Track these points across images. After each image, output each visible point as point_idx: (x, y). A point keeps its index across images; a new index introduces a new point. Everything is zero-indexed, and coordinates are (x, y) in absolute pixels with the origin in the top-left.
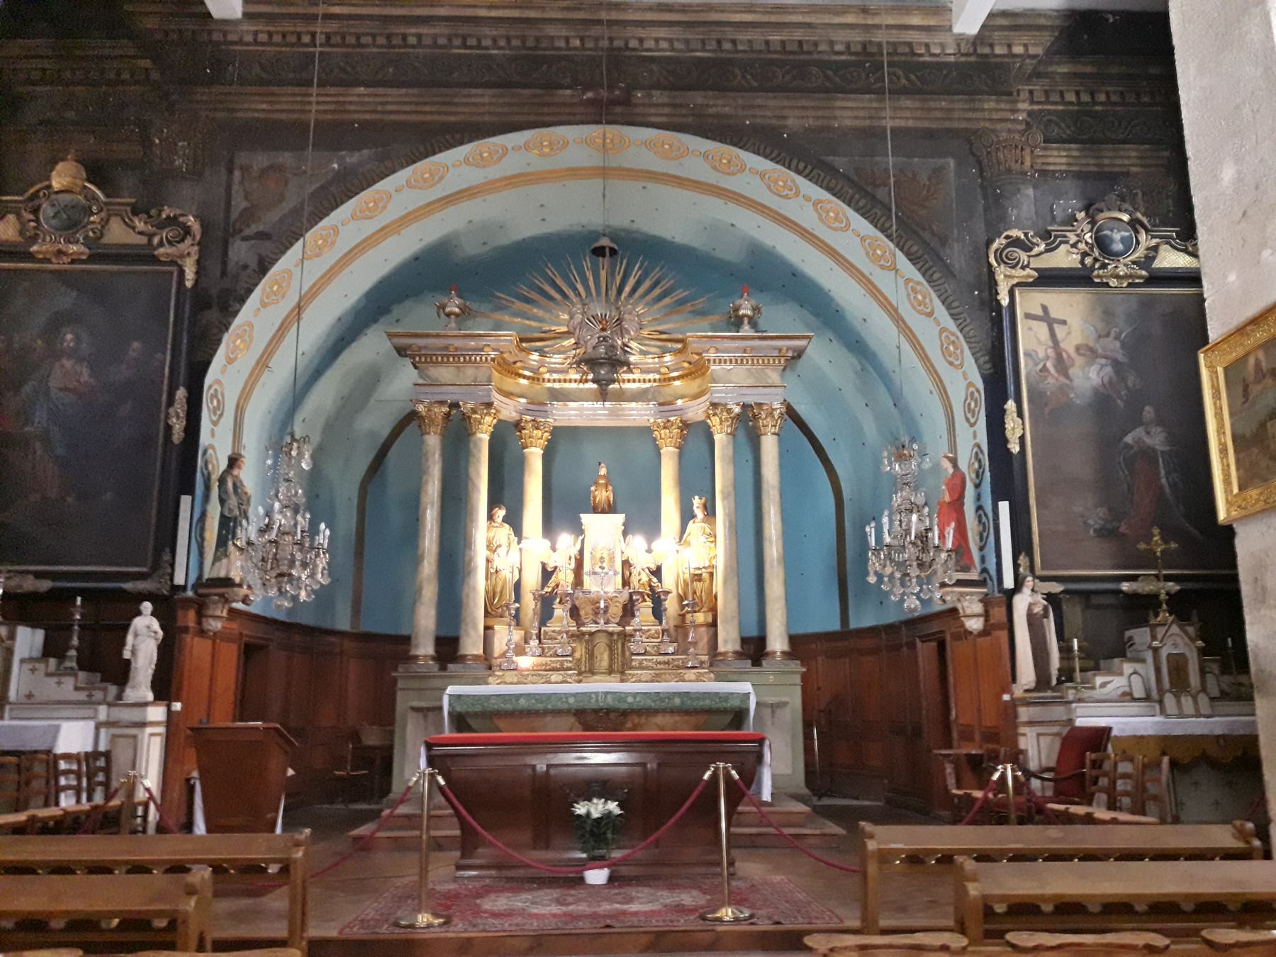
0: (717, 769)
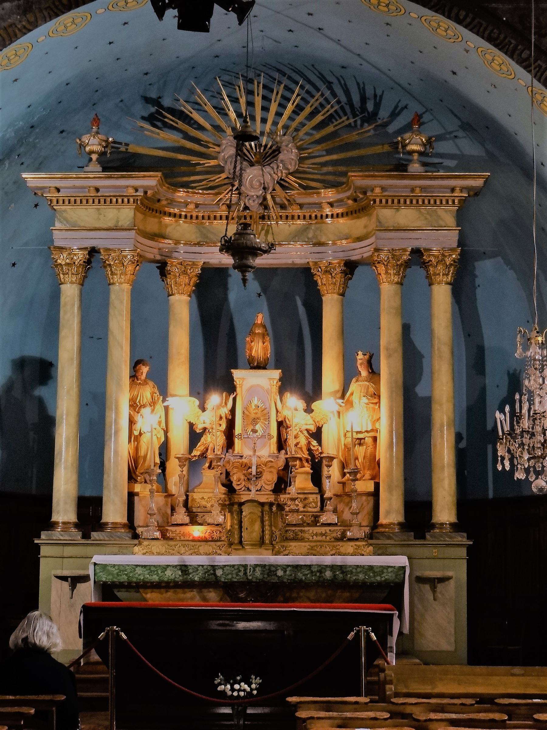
0: (359, 632)
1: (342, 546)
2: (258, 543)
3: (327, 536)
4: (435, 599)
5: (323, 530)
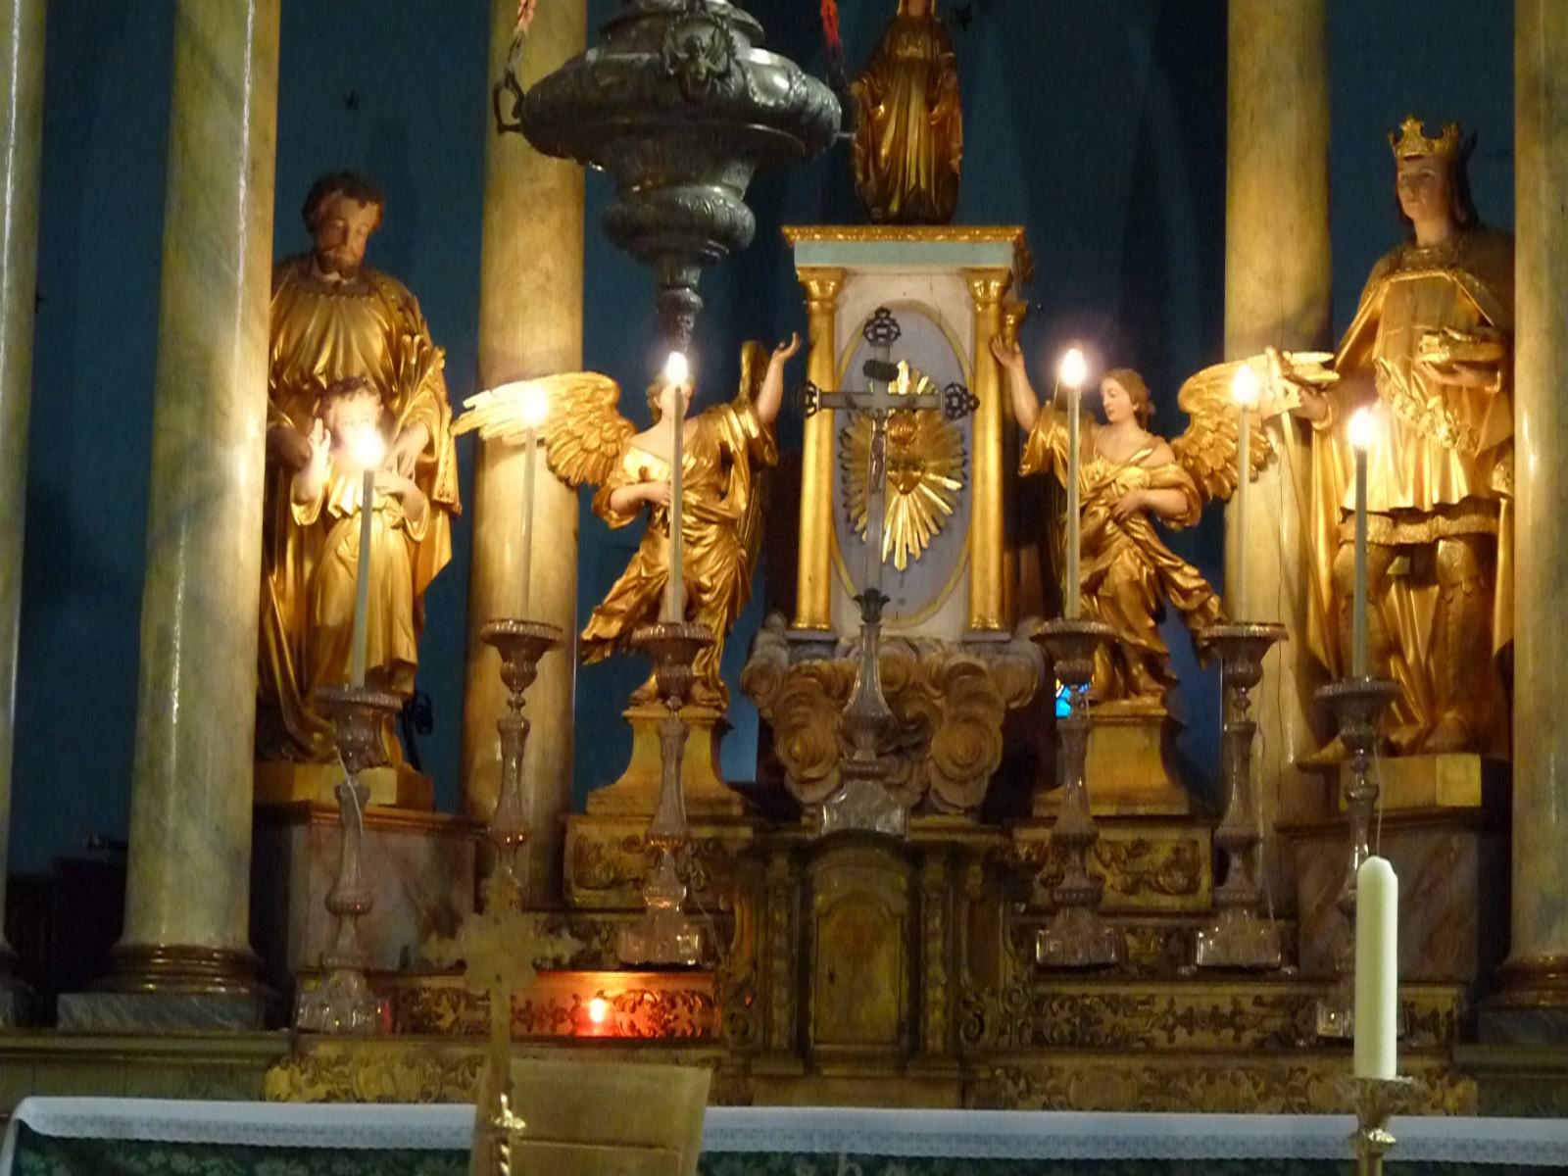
1: (1318, 1077)
2: (888, 1049)
3: (1244, 1028)
5: (1222, 996)
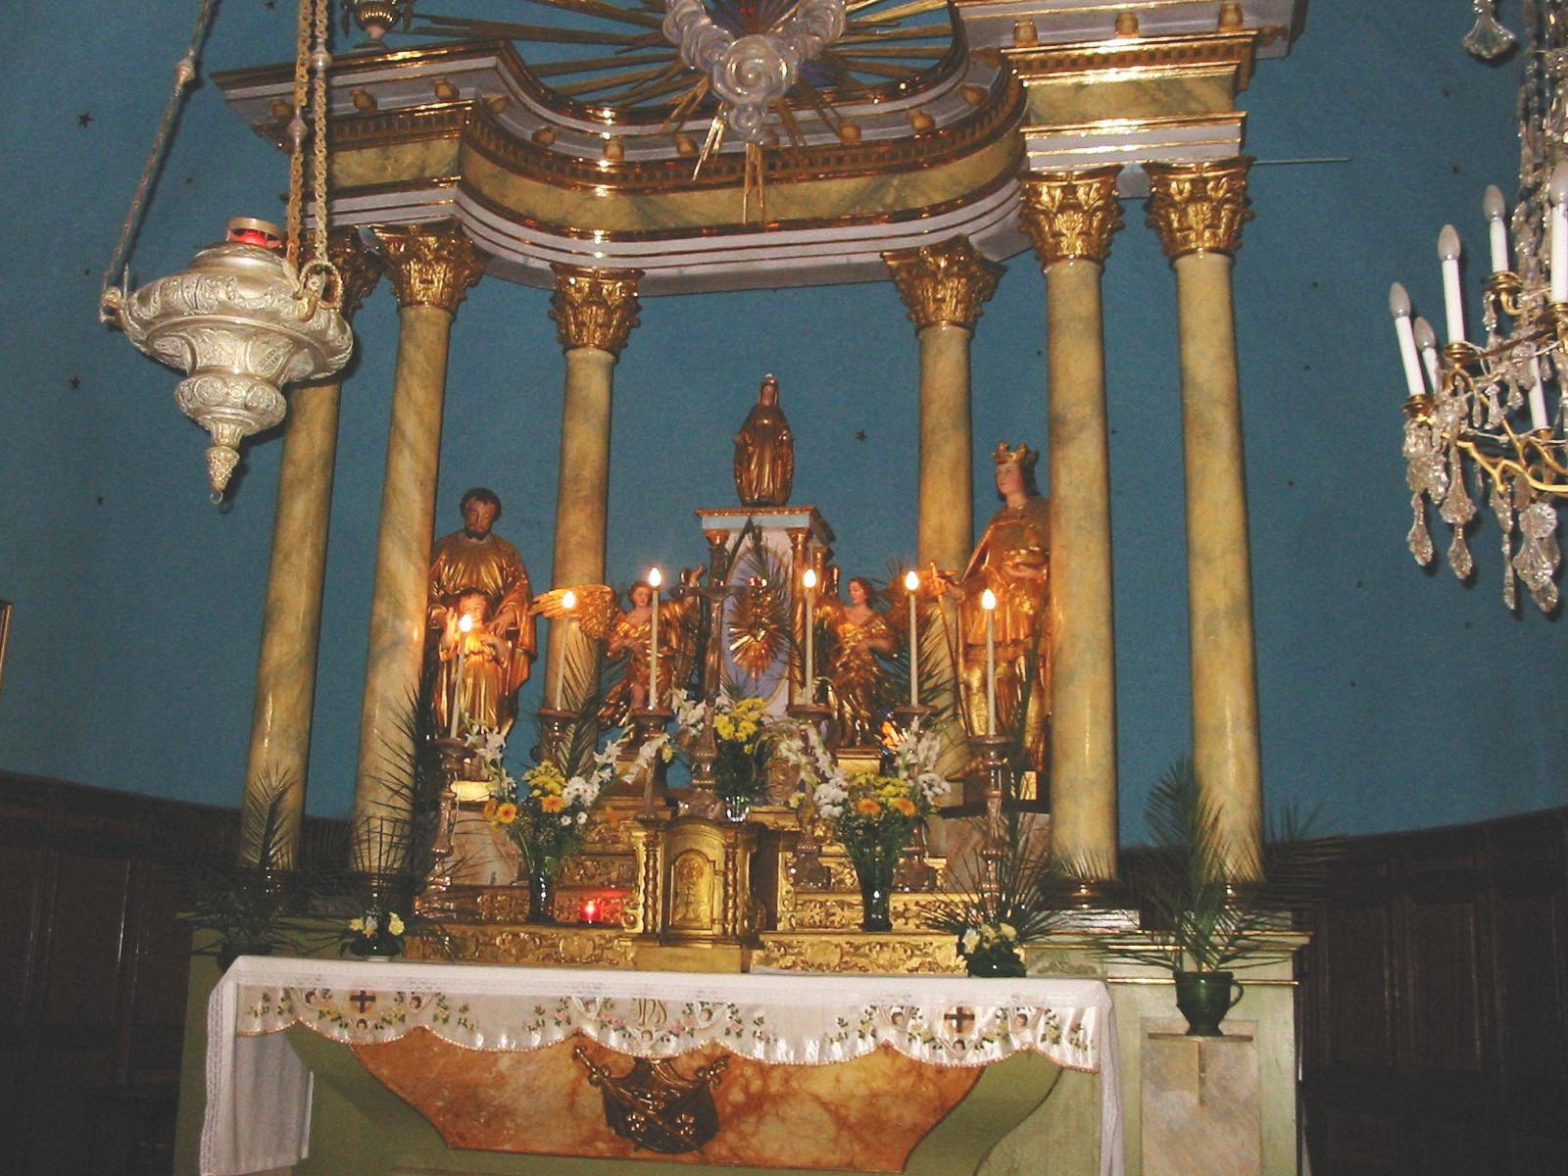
4: (494, 873)
